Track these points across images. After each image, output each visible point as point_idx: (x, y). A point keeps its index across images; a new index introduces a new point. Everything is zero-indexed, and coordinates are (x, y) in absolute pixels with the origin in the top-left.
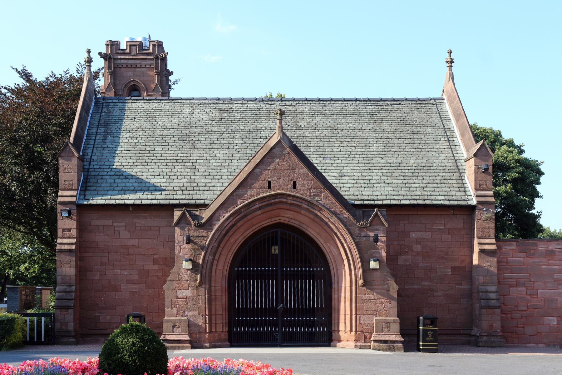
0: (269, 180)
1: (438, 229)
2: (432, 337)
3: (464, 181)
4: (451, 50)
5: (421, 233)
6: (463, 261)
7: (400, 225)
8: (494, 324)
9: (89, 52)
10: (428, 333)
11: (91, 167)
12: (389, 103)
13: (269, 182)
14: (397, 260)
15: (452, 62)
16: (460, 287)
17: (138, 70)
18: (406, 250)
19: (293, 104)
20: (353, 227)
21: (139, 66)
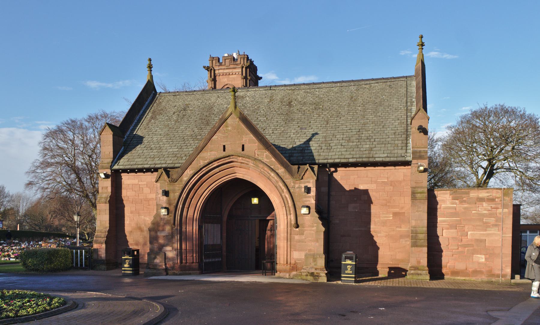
0: (224, 144)
1: (382, 182)
2: (351, 270)
3: (408, 142)
4: (422, 35)
5: (368, 185)
6: (402, 208)
7: (351, 179)
8: (421, 261)
9: (150, 60)
10: (126, 261)
11: (132, 142)
12: (368, 82)
13: (224, 146)
14: (348, 207)
15: (422, 45)
16: (400, 229)
17: (231, 76)
18: (355, 199)
19: (292, 89)
20: (288, 180)
21: (231, 73)
